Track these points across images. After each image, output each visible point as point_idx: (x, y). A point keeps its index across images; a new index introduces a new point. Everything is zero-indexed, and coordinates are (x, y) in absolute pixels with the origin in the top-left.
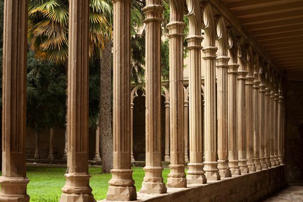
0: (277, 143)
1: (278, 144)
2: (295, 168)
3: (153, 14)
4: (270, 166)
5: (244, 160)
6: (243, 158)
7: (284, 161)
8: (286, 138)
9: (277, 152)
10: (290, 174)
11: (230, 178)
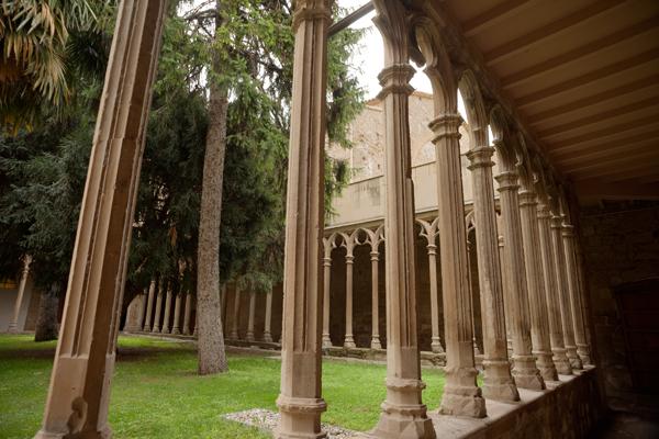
0: (568, 319)
1: (571, 318)
2: (619, 367)
3: (480, 156)
4: (555, 378)
5: (406, 382)
6: (404, 375)
7: (593, 358)
8: (589, 307)
9: (571, 337)
10: (610, 379)
11: (485, 421)
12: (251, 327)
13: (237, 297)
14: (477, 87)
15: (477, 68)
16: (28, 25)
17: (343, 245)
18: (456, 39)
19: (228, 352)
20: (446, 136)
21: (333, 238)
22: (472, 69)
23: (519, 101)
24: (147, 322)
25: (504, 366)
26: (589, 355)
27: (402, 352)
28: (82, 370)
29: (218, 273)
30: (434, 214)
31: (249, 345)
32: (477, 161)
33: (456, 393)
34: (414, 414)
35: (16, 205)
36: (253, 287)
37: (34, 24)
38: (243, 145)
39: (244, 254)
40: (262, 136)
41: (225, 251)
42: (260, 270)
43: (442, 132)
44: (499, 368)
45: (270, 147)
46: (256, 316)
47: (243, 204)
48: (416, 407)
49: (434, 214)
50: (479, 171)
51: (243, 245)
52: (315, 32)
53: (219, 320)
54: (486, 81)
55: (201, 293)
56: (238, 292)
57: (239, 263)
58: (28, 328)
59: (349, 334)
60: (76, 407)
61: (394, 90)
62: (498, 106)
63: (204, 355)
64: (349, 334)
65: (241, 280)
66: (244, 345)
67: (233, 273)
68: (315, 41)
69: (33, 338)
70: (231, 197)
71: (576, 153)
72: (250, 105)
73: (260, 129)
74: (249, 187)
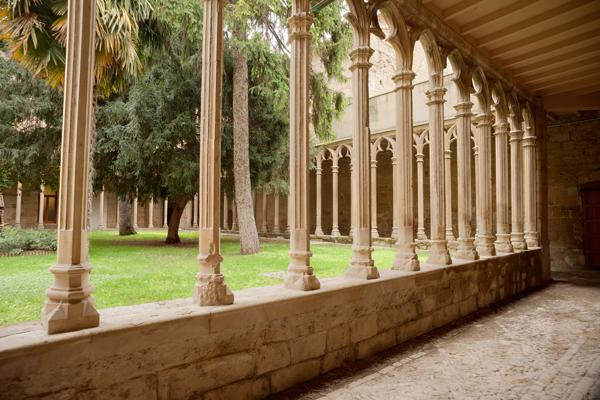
2: (575, 250)
3: (435, 95)
12: (276, 222)
13: (265, 199)
14: (434, 41)
15: (434, 26)
16: (117, 27)
17: (347, 155)
18: (414, 10)
19: (261, 242)
20: (403, 88)
21: (339, 150)
22: (430, 28)
23: (478, 41)
24: (195, 221)
25: (442, 243)
26: (539, 240)
27: (360, 231)
28: (212, 233)
29: (249, 182)
30: (422, 128)
31: (275, 236)
32: (433, 99)
33: (401, 257)
34: (366, 264)
35: (103, 139)
36: (277, 192)
37: (120, 26)
38: (262, 94)
39: (268, 167)
40: (275, 86)
41: (253, 165)
42: (281, 178)
43: (400, 84)
44: (439, 244)
45: (281, 95)
46: (280, 214)
47: (264, 127)
48: (368, 261)
49: (422, 128)
50: (434, 107)
51: (267, 160)
52: (302, 48)
53: (253, 217)
54: (444, 34)
55: (239, 198)
56: (265, 195)
57: (265, 174)
58: (111, 226)
59: (335, 225)
60: (211, 246)
61: (360, 66)
62: (456, 50)
63: (244, 242)
64: (335, 225)
65: (267, 186)
66: (272, 236)
67: (260, 182)
68: (302, 53)
69: (117, 233)
70: (255, 122)
71: (540, 75)
72: (265, 63)
73: (274, 81)
74: (269, 113)
